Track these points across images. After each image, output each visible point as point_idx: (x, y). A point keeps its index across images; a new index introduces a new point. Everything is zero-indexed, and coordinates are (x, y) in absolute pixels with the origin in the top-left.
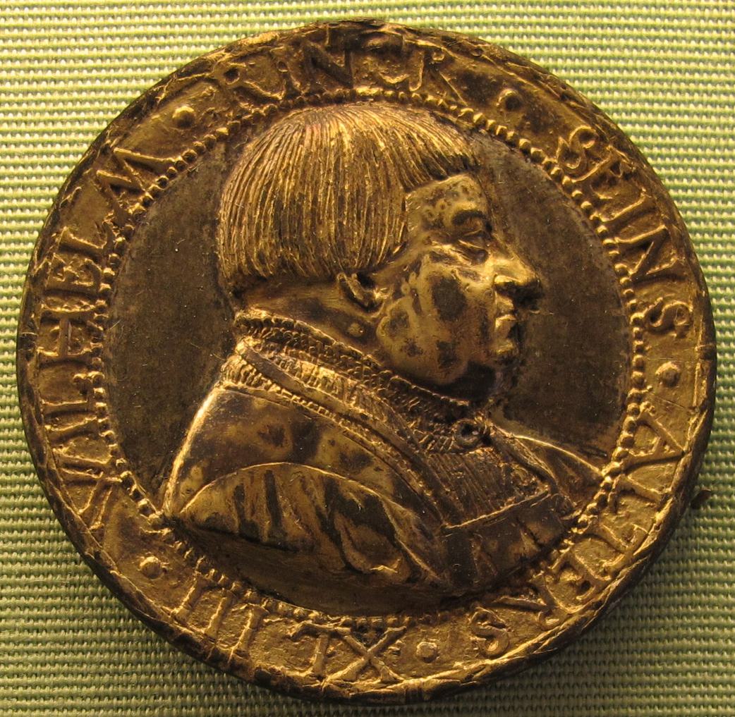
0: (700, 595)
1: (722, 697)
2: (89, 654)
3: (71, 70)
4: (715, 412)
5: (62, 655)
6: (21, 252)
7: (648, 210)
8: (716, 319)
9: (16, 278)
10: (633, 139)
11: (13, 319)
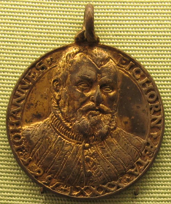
4: (165, 118)
7: (148, 82)
8: (166, 119)
9: (4, 108)
10: (142, 63)
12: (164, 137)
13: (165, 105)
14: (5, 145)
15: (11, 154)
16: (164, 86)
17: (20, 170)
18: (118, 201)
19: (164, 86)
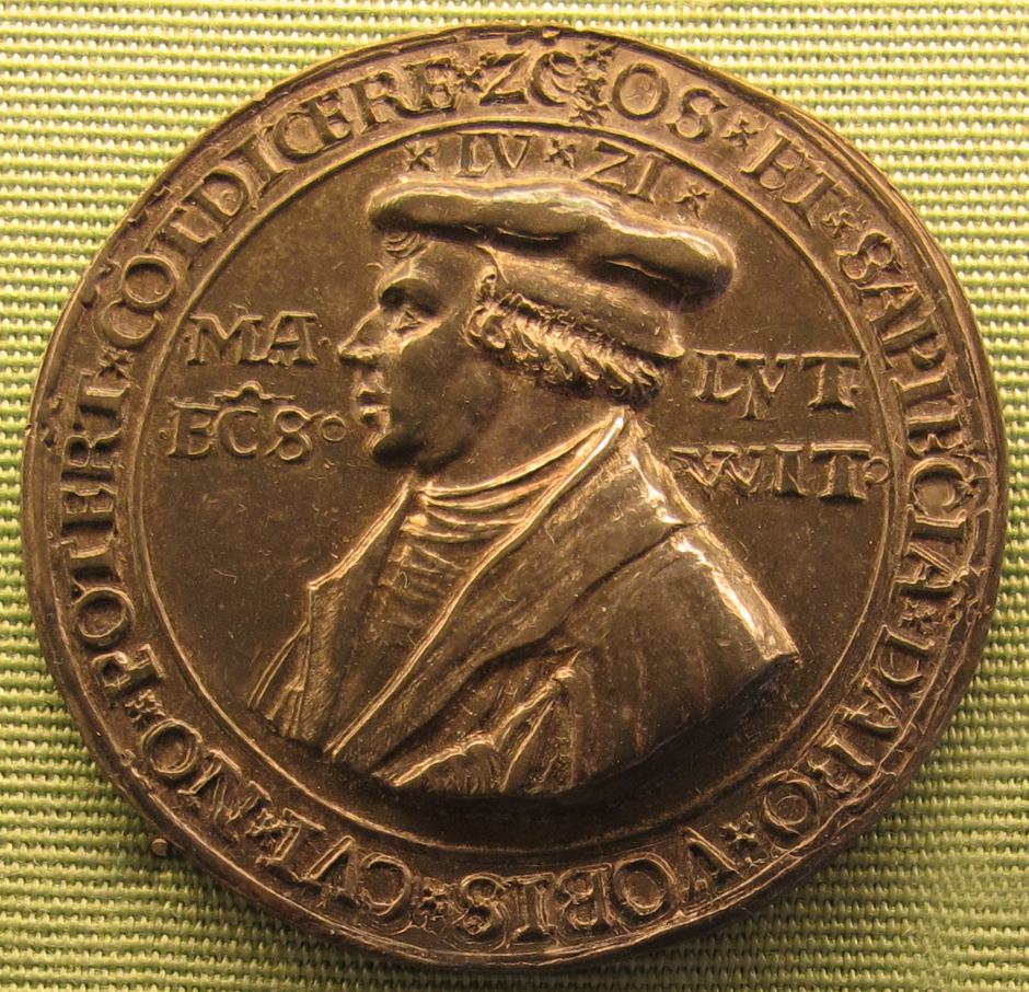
2: (72, 747)
3: (147, 58)
12: (1007, 546)
16: (1007, 327)
19: (1007, 327)
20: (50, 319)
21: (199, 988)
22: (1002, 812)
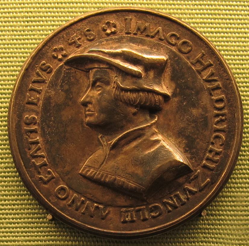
0: (239, 179)
1: (243, 93)
5: (36, 242)
6: (9, 85)
8: (244, 123)
11: (10, 90)
13: (238, 80)
14: (12, 172)
15: (20, 182)
17: (72, 240)
18: (138, 242)
20: (12, 84)
21: (46, 245)
22: (242, 215)
